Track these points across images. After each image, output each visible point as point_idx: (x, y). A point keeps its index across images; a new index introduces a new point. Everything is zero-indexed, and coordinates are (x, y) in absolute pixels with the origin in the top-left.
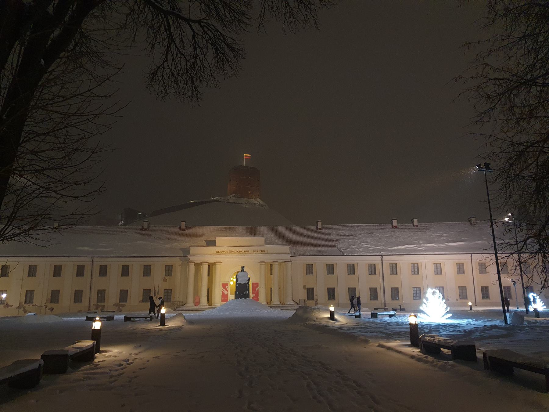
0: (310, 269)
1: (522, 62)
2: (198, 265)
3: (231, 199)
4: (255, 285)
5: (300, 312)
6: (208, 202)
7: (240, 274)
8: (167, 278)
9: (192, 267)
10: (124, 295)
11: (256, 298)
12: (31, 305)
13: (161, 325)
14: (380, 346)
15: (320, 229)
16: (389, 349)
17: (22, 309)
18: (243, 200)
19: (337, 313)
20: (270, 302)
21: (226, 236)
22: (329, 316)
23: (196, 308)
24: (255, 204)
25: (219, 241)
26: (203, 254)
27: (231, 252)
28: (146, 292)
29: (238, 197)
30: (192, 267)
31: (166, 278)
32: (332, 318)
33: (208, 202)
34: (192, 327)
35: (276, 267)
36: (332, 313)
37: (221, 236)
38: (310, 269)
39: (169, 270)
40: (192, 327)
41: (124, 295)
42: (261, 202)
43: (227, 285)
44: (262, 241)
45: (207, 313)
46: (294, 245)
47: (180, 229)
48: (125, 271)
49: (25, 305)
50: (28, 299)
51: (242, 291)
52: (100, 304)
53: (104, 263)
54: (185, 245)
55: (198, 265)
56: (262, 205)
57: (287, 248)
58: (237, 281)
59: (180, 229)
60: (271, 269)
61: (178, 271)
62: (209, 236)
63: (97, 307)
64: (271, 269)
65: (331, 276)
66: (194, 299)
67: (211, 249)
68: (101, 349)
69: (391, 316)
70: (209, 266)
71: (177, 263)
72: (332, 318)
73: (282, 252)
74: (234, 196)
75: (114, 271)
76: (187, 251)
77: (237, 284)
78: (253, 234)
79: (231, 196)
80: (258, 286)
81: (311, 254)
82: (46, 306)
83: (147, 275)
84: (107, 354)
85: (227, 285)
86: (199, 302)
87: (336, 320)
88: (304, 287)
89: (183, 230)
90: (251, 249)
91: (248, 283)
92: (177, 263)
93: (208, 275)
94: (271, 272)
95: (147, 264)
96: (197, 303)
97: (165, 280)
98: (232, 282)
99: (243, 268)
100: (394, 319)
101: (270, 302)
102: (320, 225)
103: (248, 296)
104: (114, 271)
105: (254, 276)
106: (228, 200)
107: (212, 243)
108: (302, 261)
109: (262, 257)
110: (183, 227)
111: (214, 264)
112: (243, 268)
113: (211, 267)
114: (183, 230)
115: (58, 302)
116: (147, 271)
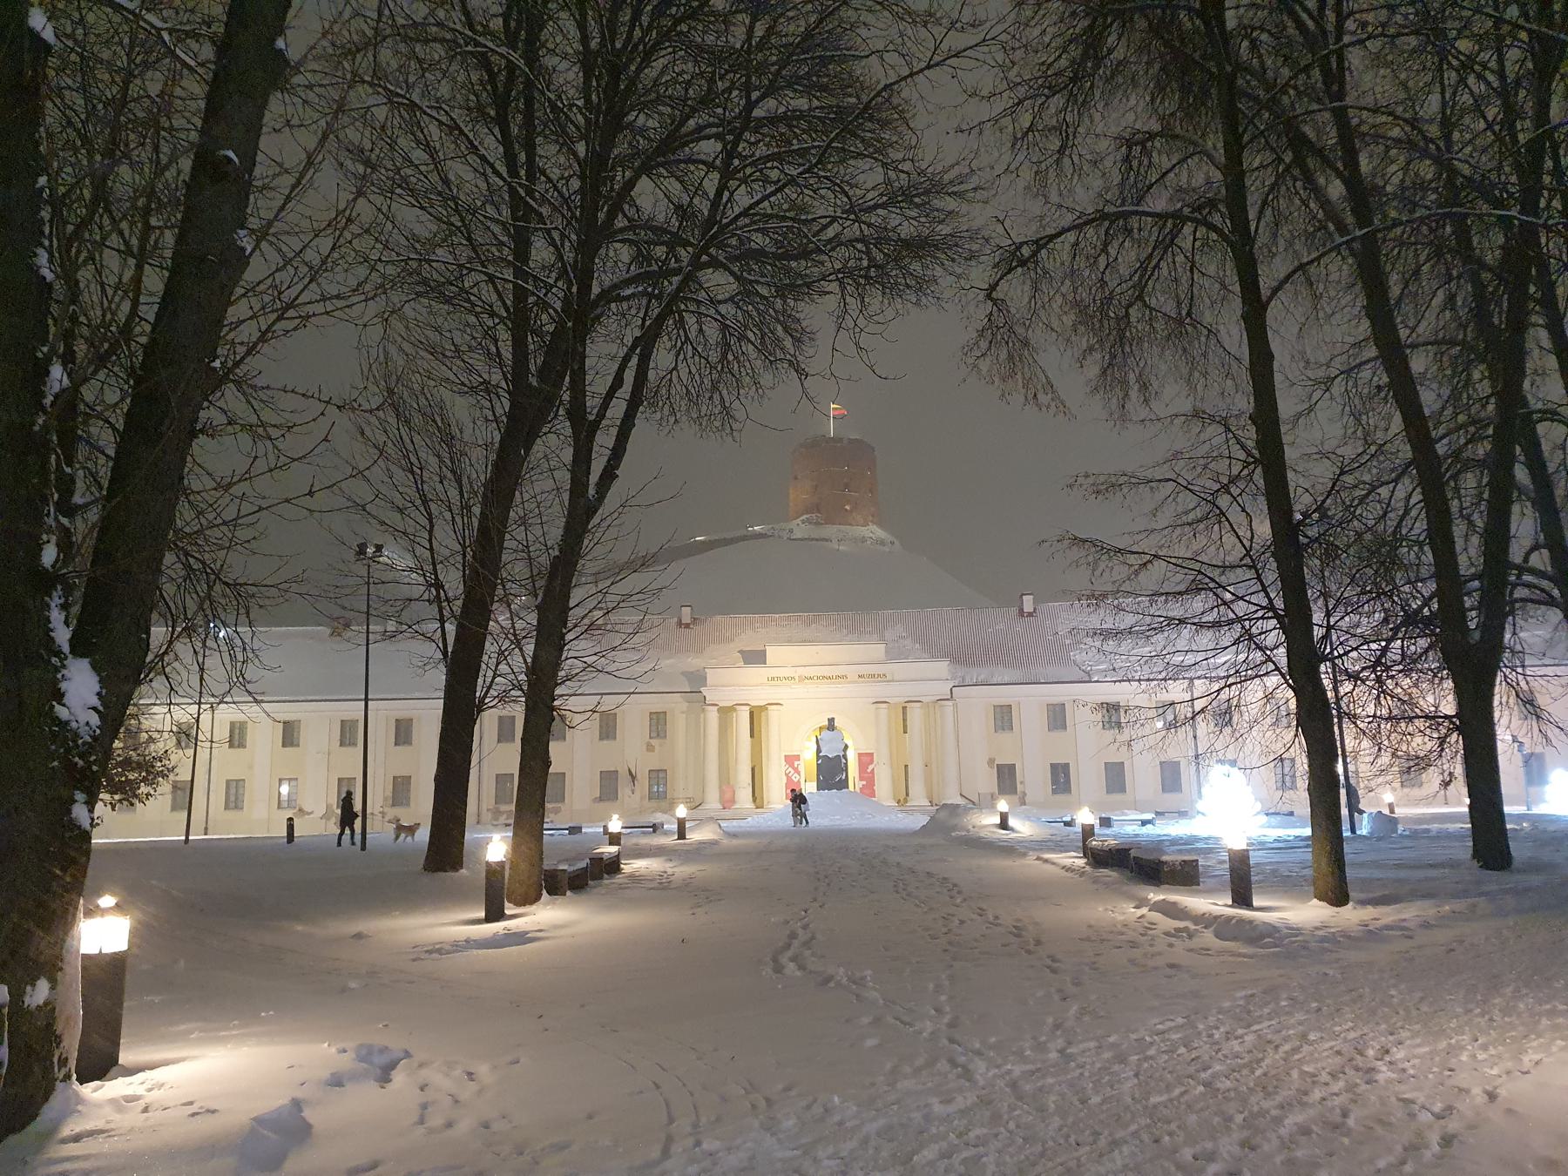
0: (1004, 717)
2: (726, 712)
4: (865, 759)
5: (943, 815)
6: (744, 538)
7: (826, 733)
9: (713, 715)
11: (869, 789)
13: (489, 919)
14: (1038, 859)
15: (1030, 614)
16: (1046, 861)
18: (831, 531)
19: (1016, 815)
20: (903, 801)
21: (790, 641)
22: (998, 821)
23: (727, 813)
24: (864, 540)
25: (773, 653)
26: (737, 685)
27: (802, 679)
29: (817, 524)
30: (713, 715)
31: (653, 742)
32: (1004, 825)
33: (744, 538)
34: (735, 842)
35: (915, 714)
36: (1004, 818)
37: (778, 641)
38: (1004, 717)
39: (658, 724)
40: (735, 842)
42: (880, 533)
43: (797, 758)
44: (878, 650)
45: (756, 821)
46: (960, 658)
47: (680, 624)
50: (232, 798)
51: (831, 772)
54: (693, 662)
55: (726, 712)
56: (882, 543)
57: (942, 667)
58: (819, 750)
59: (680, 624)
60: (905, 720)
61: (679, 726)
62: (748, 640)
64: (905, 720)
66: (722, 792)
67: (755, 673)
68: (125, 1057)
69: (1144, 823)
70: (752, 714)
71: (675, 706)
72: (1004, 825)
73: (929, 676)
74: (809, 521)
76: (697, 680)
77: (818, 757)
78: (857, 632)
80: (872, 762)
81: (1006, 680)
82: (383, 813)
83: (607, 737)
85: (797, 758)
86: (733, 801)
87: (1012, 830)
88: (991, 761)
89: (687, 626)
90: (852, 671)
91: (845, 757)
92: (675, 706)
93: (752, 736)
94: (905, 727)
96: (728, 802)
97: (650, 748)
98: (809, 757)
99: (831, 720)
100: (1149, 830)
101: (906, 801)
102: (1028, 603)
103: (843, 784)
105: (855, 744)
106: (791, 531)
107: (756, 657)
108: (980, 700)
109: (880, 690)
110: (686, 620)
111: (763, 708)
112: (831, 720)
113: (756, 716)
114: (687, 626)
115: (408, 805)
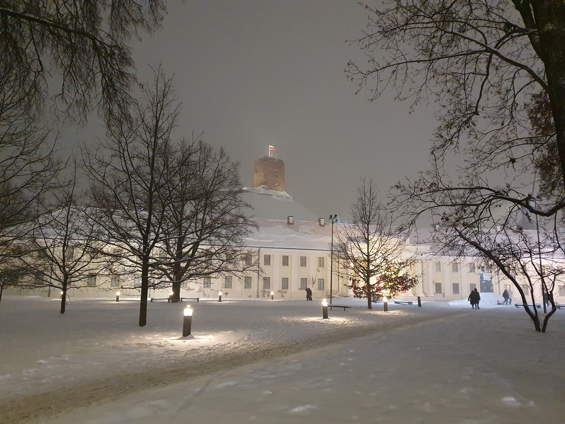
1: (44, 9)
3: (261, 189)
8: (320, 268)
10: (285, 283)
12: (209, 289)
17: (202, 292)
18: (271, 192)
24: (282, 196)
28: (304, 281)
29: (266, 189)
41: (285, 283)
42: (287, 195)
48: (286, 261)
49: (204, 289)
52: (266, 290)
53: (268, 254)
56: (288, 198)
63: (264, 292)
65: (455, 273)
75: (277, 260)
79: (260, 187)
83: (267, 264)
84: (200, 340)
88: (433, 282)
89: (323, 226)
95: (303, 255)
97: (318, 271)
104: (277, 260)
110: (322, 223)
114: (323, 226)
116: (303, 262)
